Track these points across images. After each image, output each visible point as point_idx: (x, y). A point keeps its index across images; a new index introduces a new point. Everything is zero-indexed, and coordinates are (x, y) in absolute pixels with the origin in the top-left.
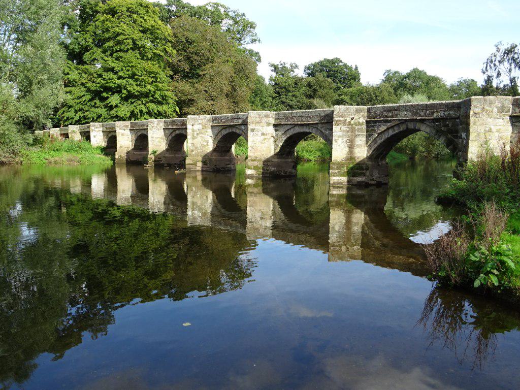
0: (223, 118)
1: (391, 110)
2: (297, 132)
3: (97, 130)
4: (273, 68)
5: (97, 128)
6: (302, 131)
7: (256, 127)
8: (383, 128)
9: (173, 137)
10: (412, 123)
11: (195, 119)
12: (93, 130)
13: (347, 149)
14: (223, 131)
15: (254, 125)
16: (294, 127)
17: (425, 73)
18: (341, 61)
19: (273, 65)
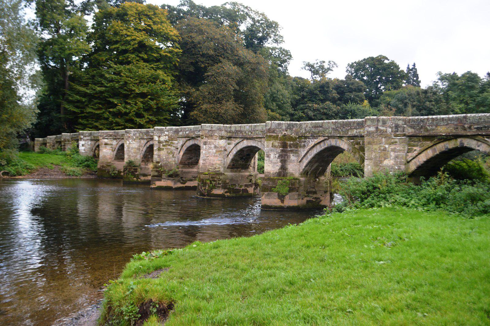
0: (187, 129)
1: (318, 127)
2: (246, 146)
3: (85, 138)
4: (411, 67)
5: (85, 137)
6: (249, 145)
7: (209, 140)
8: (312, 142)
9: (454, 166)
10: (334, 140)
11: (161, 130)
12: (81, 139)
13: (280, 164)
14: (187, 143)
15: (207, 138)
16: (243, 140)
17: (338, 80)
18: (387, 59)
19: (308, 65)
